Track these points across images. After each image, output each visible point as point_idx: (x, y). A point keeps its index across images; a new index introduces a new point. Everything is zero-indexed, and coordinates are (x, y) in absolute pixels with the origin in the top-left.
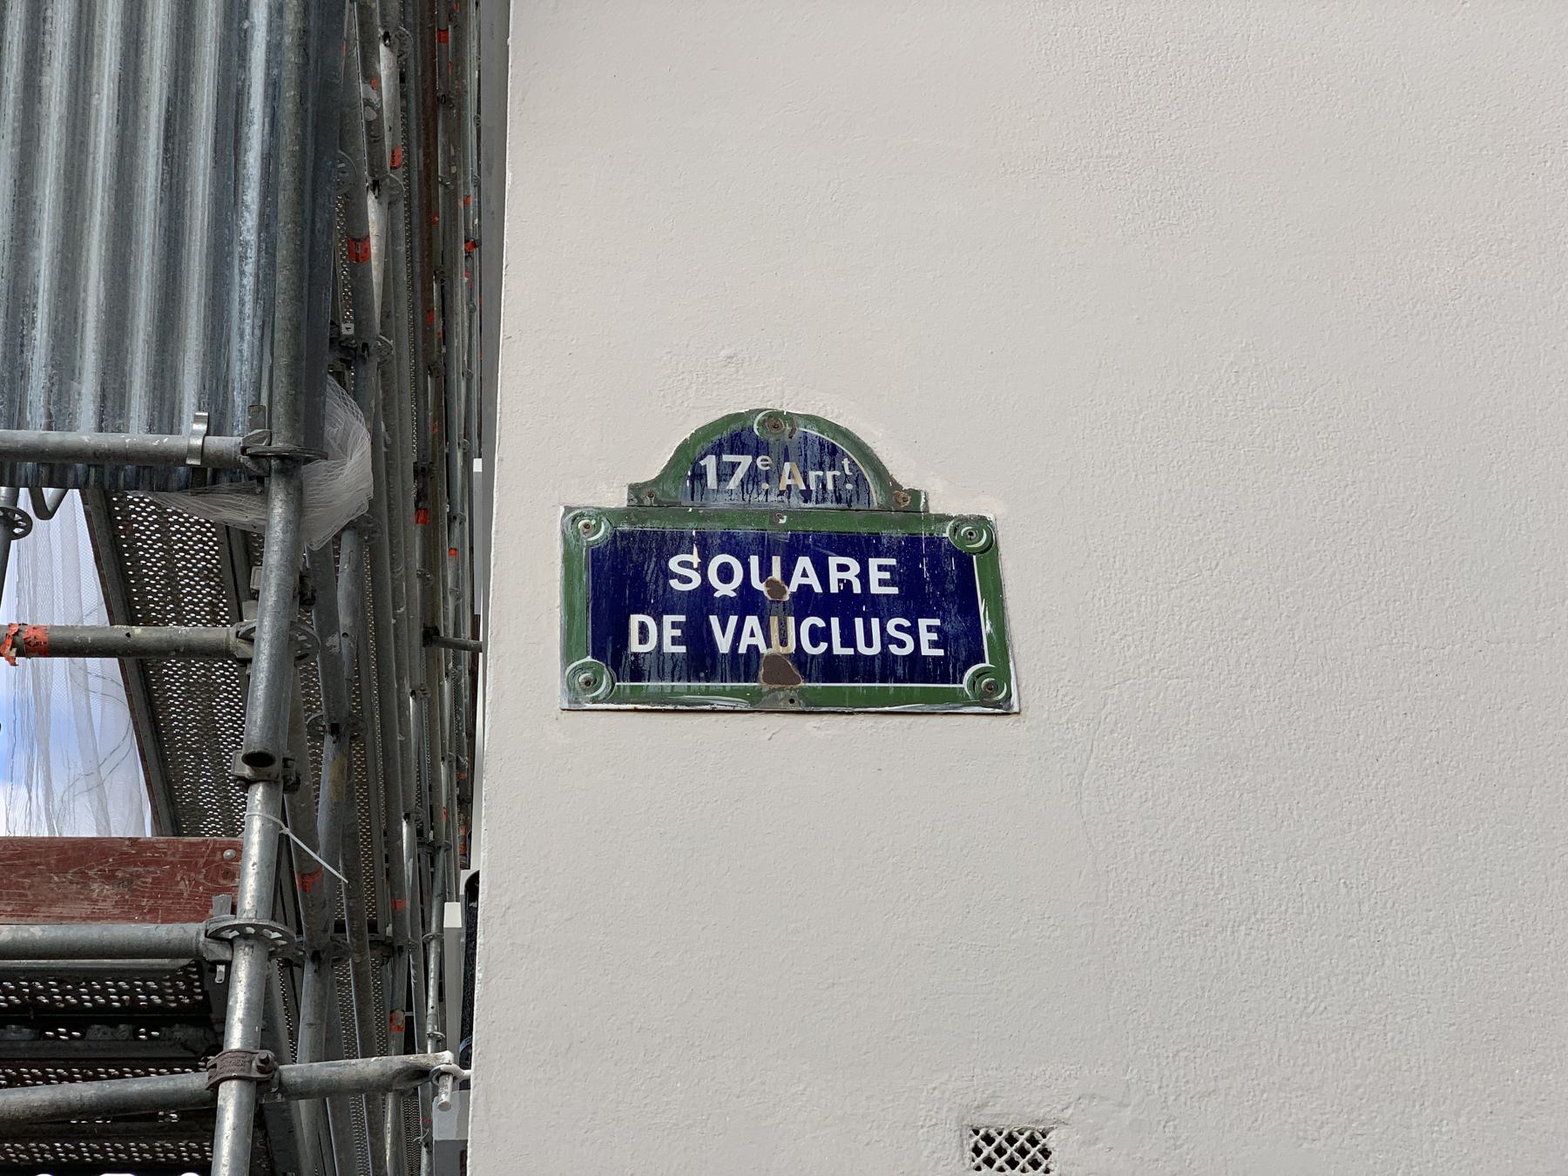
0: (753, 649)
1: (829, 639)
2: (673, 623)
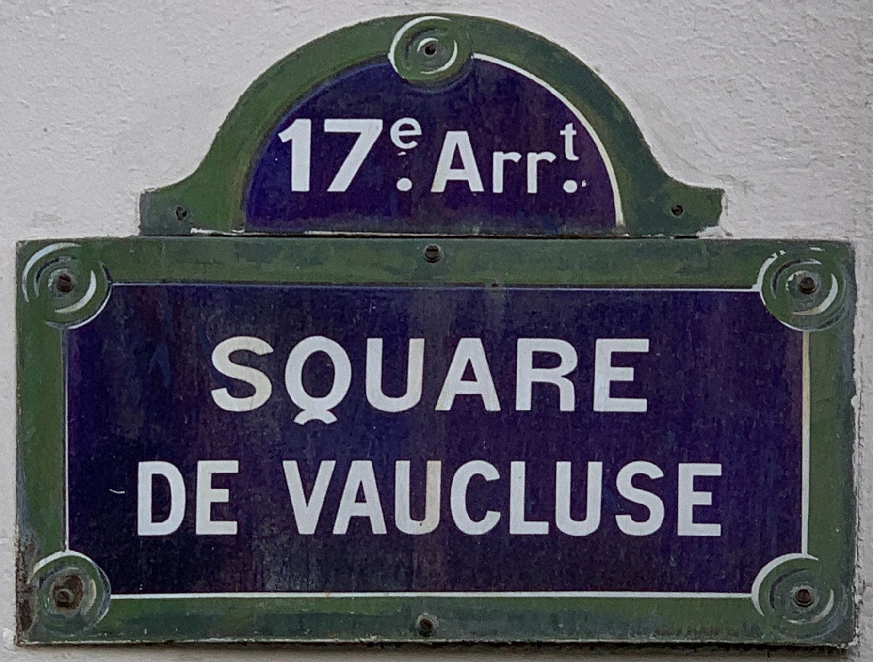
0: (359, 524)
1: (505, 510)
2: (215, 476)
